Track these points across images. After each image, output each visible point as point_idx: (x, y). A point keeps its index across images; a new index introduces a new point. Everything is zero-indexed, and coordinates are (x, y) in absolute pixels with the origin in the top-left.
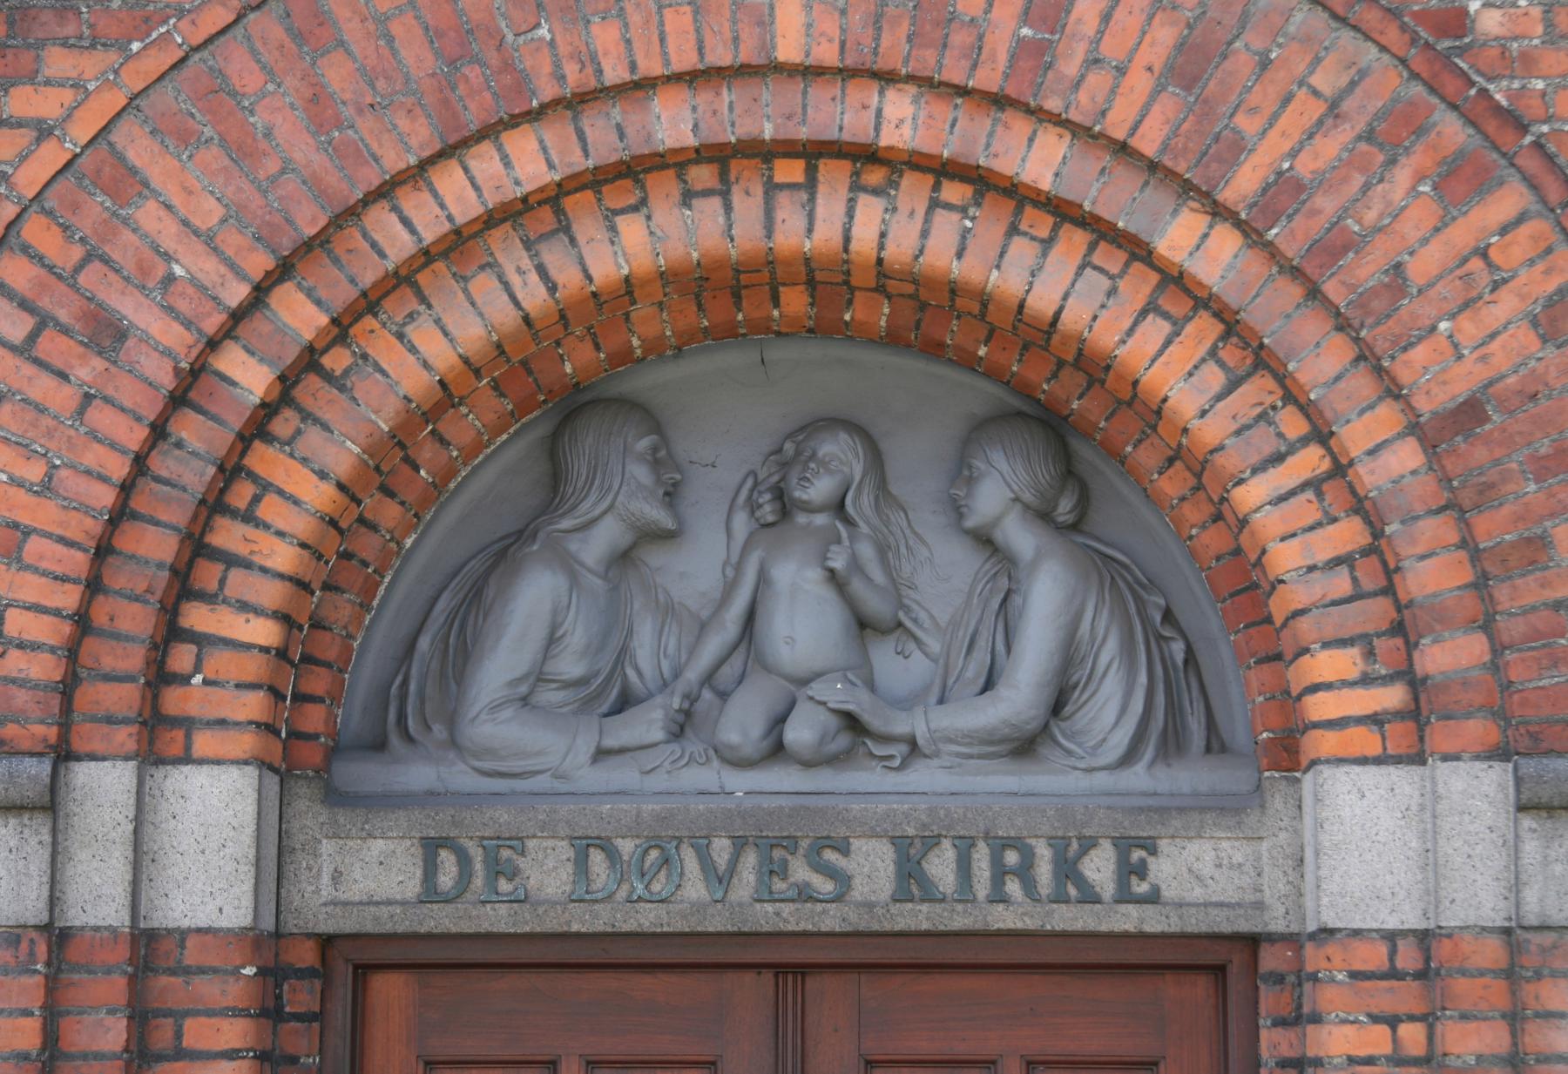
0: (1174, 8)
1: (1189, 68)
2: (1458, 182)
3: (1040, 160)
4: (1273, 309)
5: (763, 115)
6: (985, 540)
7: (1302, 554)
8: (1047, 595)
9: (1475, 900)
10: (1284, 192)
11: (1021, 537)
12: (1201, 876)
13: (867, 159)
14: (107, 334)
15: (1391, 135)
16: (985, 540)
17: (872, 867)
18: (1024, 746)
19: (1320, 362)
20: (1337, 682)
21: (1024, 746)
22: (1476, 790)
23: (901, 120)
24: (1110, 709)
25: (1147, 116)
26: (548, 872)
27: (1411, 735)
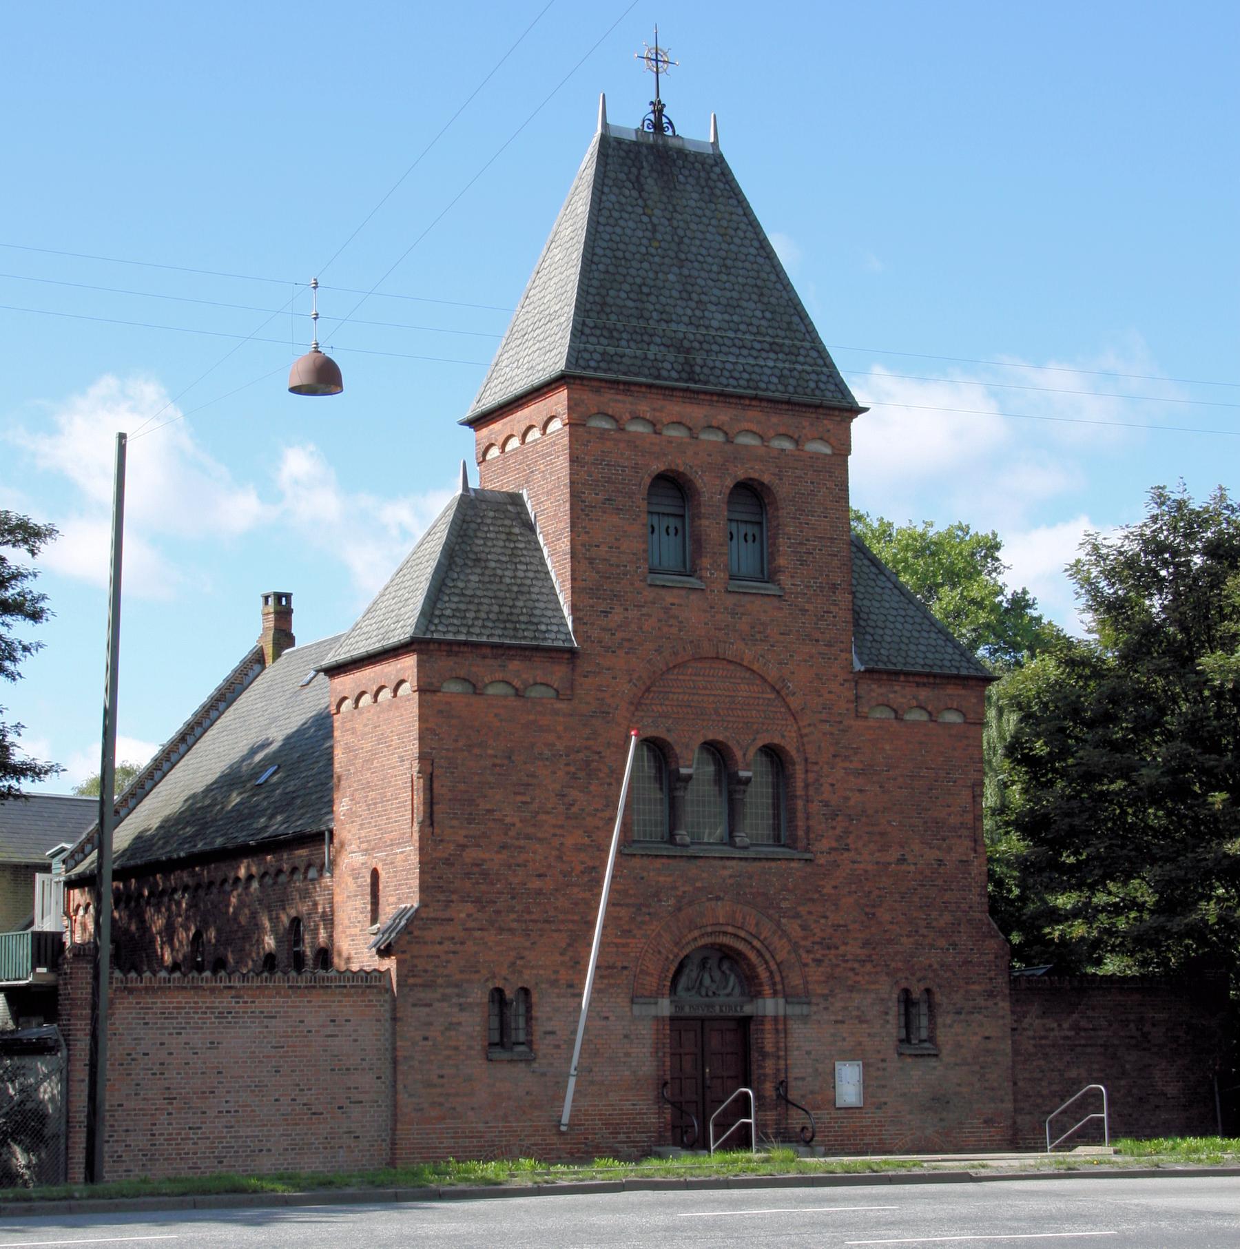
0: (1014, 1029)
1: (757, 924)
2: (780, 938)
3: (742, 934)
4: (763, 950)
5: (717, 929)
6: (723, 972)
7: (764, 975)
8: (732, 979)
9: (781, 1012)
10: (765, 938)
11: (728, 972)
12: (748, 1010)
13: (725, 933)
14: (659, 952)
15: (774, 933)
16: (723, 972)
17: (717, 1008)
18: (728, 995)
19: (768, 956)
20: (767, 990)
21: (728, 995)
22: (781, 1001)
23: (730, 929)
24: (737, 991)
25: (753, 930)
26: (687, 1009)
27: (775, 994)
